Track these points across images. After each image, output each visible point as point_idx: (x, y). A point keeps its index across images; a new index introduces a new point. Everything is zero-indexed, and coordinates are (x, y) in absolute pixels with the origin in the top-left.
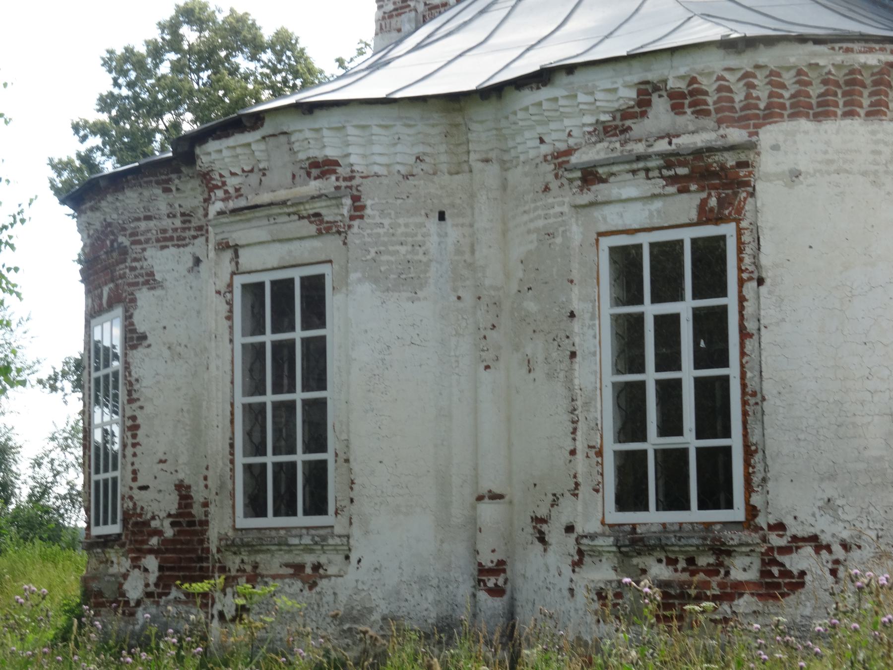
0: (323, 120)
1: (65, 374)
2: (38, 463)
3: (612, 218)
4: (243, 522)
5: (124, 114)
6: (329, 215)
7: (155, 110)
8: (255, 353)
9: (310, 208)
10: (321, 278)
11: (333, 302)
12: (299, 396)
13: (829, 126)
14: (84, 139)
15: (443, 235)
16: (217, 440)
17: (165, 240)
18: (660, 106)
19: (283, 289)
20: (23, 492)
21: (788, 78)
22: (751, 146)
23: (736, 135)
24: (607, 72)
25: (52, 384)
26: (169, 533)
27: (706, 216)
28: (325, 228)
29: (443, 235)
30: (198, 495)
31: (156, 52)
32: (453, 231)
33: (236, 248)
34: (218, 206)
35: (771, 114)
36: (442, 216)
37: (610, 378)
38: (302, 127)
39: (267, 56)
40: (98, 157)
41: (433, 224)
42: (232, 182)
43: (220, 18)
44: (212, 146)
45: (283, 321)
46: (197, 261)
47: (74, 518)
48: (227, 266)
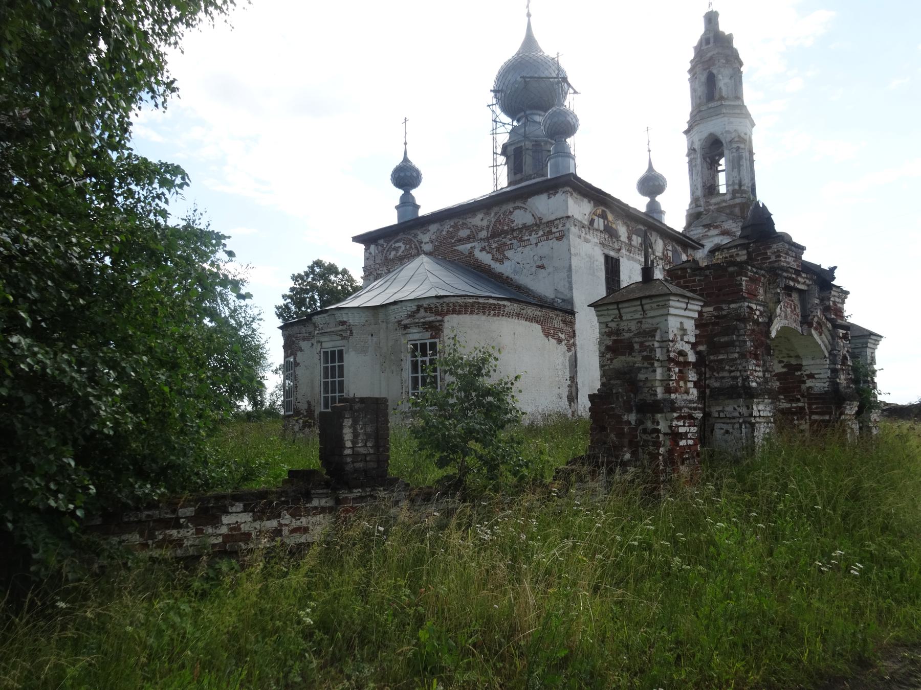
0: (343, 312)
1: (280, 369)
2: (272, 395)
3: (411, 337)
4: (323, 410)
5: (297, 293)
6: (344, 335)
7: (306, 291)
8: (326, 369)
9: (340, 333)
10: (342, 350)
11: (345, 356)
12: (337, 379)
13: (460, 316)
14: (285, 300)
15: (372, 340)
16: (317, 390)
17: (304, 339)
18: (422, 311)
19: (333, 353)
20: (267, 404)
21: (451, 305)
22: (442, 321)
23: (439, 318)
24: (410, 302)
25: (276, 372)
26: (305, 414)
27: (432, 337)
28: (343, 338)
29: (372, 340)
30: (313, 404)
31: (307, 274)
32: (375, 339)
33: (322, 342)
34: (317, 332)
35: (447, 313)
36: (372, 335)
37: (410, 375)
38: (338, 313)
39: (340, 276)
40: (290, 305)
41: (370, 337)
42: (321, 326)
43: (326, 265)
44: (316, 317)
45: (333, 361)
46: (313, 345)
47: (382, 590)
48: (319, 347)
